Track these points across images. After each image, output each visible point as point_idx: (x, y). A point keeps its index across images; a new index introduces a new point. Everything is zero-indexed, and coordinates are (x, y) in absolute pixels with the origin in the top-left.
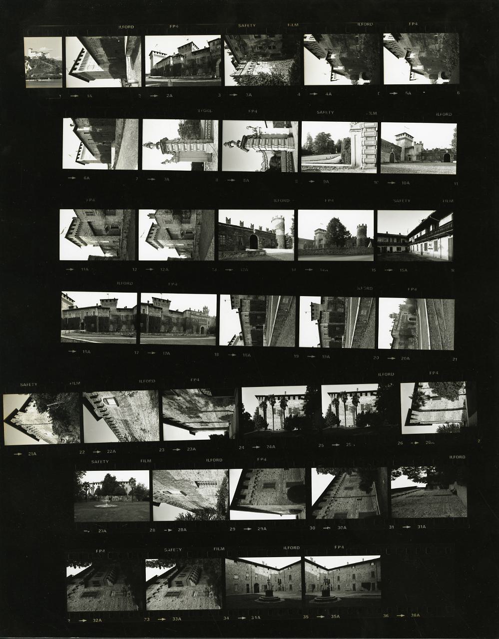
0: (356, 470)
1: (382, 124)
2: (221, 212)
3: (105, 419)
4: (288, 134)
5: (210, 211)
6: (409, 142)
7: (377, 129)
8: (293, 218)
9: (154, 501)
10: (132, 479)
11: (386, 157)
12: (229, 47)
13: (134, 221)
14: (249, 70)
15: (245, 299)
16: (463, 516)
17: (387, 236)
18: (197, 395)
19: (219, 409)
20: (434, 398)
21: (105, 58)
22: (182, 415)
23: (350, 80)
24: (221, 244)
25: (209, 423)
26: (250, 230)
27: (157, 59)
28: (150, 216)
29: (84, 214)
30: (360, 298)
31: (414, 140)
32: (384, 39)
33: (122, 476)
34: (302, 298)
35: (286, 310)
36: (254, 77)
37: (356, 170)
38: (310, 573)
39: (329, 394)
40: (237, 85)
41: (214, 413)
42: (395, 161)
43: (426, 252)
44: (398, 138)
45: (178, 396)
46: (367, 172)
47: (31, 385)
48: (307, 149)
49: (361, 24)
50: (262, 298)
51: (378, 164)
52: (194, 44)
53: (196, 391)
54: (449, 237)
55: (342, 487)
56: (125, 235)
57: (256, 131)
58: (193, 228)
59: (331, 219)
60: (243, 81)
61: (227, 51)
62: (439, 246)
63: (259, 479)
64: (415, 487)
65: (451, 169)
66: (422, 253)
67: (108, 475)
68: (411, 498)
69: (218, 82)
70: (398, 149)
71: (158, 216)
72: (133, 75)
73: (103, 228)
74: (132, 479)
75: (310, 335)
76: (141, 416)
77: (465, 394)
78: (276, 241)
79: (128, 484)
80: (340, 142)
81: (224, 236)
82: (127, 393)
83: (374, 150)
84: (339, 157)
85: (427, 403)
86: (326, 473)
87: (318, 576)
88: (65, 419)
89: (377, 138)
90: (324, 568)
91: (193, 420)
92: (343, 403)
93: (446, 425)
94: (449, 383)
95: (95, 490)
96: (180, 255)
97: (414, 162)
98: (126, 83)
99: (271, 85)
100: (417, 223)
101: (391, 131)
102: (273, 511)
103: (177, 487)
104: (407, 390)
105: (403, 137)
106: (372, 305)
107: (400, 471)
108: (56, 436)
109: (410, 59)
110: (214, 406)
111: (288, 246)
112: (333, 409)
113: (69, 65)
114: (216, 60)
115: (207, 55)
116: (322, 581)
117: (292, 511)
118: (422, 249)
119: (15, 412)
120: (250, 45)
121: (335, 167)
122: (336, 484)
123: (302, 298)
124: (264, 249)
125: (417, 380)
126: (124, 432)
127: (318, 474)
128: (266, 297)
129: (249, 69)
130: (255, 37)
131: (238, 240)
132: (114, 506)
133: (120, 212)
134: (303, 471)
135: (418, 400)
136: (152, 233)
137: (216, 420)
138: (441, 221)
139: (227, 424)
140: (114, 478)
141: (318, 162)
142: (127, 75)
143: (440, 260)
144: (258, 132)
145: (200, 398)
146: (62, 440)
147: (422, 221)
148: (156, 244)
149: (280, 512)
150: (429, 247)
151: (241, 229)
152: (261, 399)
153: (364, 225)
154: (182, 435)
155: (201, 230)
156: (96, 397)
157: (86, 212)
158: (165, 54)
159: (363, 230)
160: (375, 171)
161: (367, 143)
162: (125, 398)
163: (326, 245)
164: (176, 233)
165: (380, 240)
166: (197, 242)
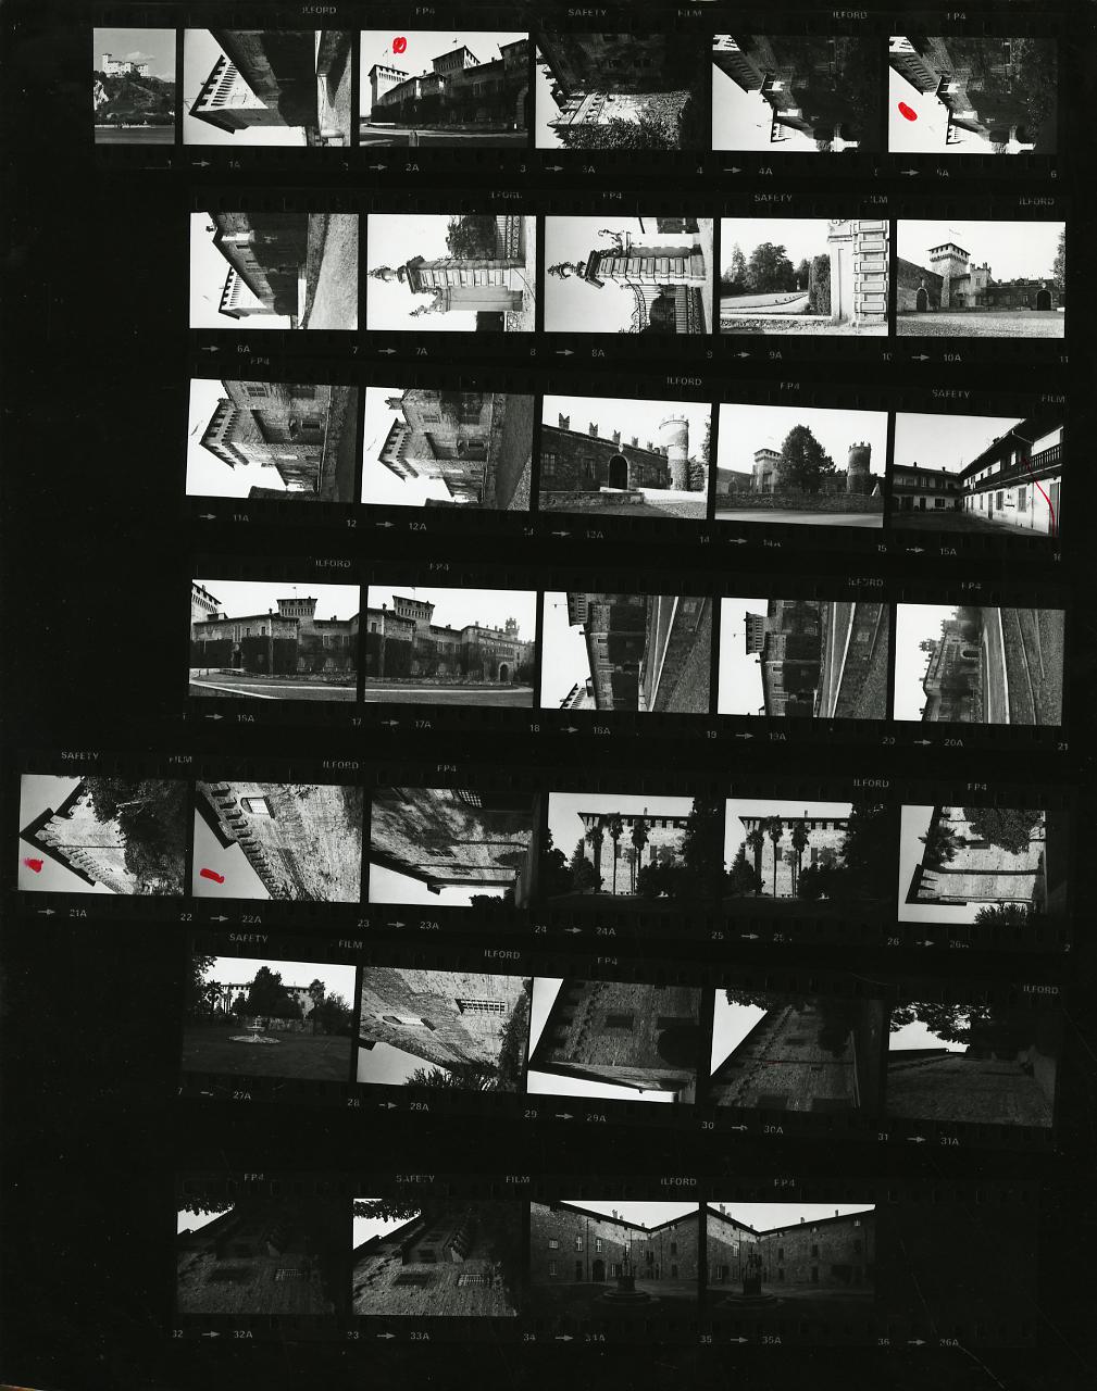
0: (815, 1001)
1: (900, 222)
2: (548, 400)
3: (243, 846)
4: (691, 247)
5: (524, 397)
6: (961, 264)
7: (888, 236)
8: (709, 421)
9: (361, 1036)
10: (317, 982)
11: (908, 299)
12: (546, 60)
13: (355, 414)
14: (589, 114)
15: (599, 603)
16: (1044, 1125)
17: (914, 471)
18: (449, 804)
19: (497, 838)
20: (975, 844)
21: (270, 80)
22: (412, 848)
23: (815, 141)
24: (546, 473)
25: (472, 868)
26: (611, 446)
27: (386, 85)
28: (392, 402)
29: (244, 391)
30: (854, 605)
31: (971, 260)
32: (892, 49)
33: (295, 974)
34: (725, 602)
35: (691, 630)
36: (602, 128)
37: (842, 327)
38: (717, 1241)
39: (742, 819)
40: (562, 146)
41: (485, 847)
42: (929, 307)
43: (1000, 511)
44: (935, 255)
45: (408, 803)
46: (867, 332)
47: (86, 756)
48: (732, 280)
49: (840, 15)
50: (635, 600)
51: (891, 316)
52: (468, 52)
53: (449, 794)
54: (1051, 481)
55: (781, 1038)
56: (333, 443)
57: (619, 240)
59: (791, 428)
60: (576, 138)
61: (541, 70)
62: (1028, 500)
63: (598, 1005)
64: (943, 1051)
65: (1051, 326)
66: (990, 514)
67: (265, 970)
68: (931, 1074)
69: (519, 139)
70: (935, 279)
71: (408, 404)
72: (331, 119)
73: (284, 425)
74: (317, 982)
75: (742, 688)
76: (323, 844)
77: (1042, 840)
78: (667, 472)
79: (308, 993)
80: (806, 265)
81: (553, 457)
82: (293, 789)
83: (881, 284)
84: (803, 300)
85: (957, 854)
86: (747, 1004)
87: (737, 1247)
88: (156, 840)
89: (888, 255)
90: (750, 1230)
91: (437, 859)
92: (772, 843)
93: (996, 906)
94: (1009, 811)
95: (233, 1000)
96: (452, 495)
97: (970, 310)
98: (317, 138)
99: (635, 147)
100: (984, 446)
101: (920, 240)
102: (623, 1080)
103: (414, 1009)
104: (915, 821)
105: (945, 252)
106: (882, 621)
107: (912, 1011)
108: (133, 877)
109: (947, 95)
110: (485, 831)
111: (693, 486)
112: (750, 854)
113: (191, 93)
114: (519, 88)
115: (498, 77)
116: (745, 1260)
117: (666, 1085)
118: (990, 506)
119: (47, 816)
120: (593, 57)
121: (796, 322)
122: (767, 1030)
123: (725, 602)
124: (641, 490)
125: (939, 801)
126: (281, 876)
127: (730, 1003)
128: (646, 601)
129: (591, 111)
130: (606, 39)
131: (583, 467)
132: (271, 1040)
133: (324, 390)
134: (697, 993)
135: (938, 844)
136: (394, 443)
137: (488, 862)
138: (1035, 443)
139: (513, 874)
140: (278, 977)
141: (759, 310)
142: (320, 118)
143: (1030, 533)
144: (624, 243)
145: (456, 811)
146: (144, 885)
147: (994, 441)
148: (401, 468)
149: (638, 1084)
150: (1006, 501)
151: (590, 443)
152: (591, 821)
153: (866, 445)
154: (411, 892)
155: (503, 441)
156: (225, 793)
157: (249, 389)
158: (404, 74)
159: (862, 456)
160: (883, 331)
161: (865, 266)
162: (289, 800)
163: (779, 486)
164: (447, 444)
165: (899, 481)
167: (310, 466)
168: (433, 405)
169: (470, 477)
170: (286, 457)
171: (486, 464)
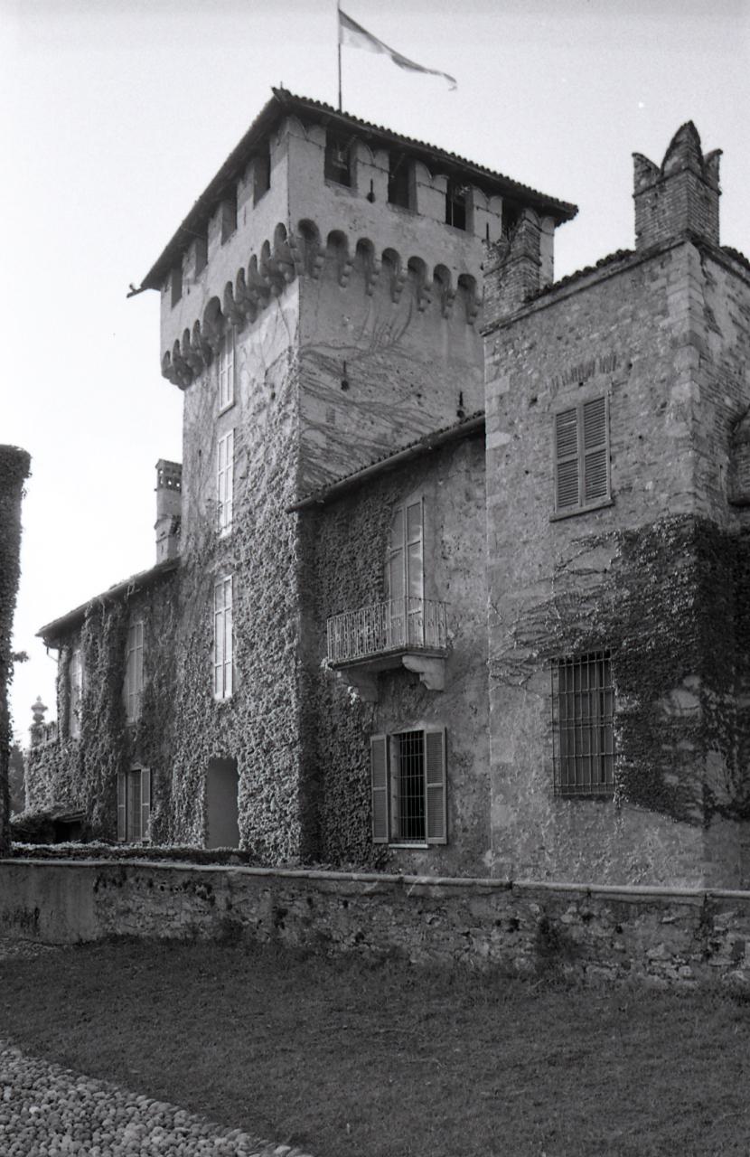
29: (581, 375)
58: (482, 840)
96: (60, 634)
136: (401, 196)
155: (448, 979)
164: (409, 580)
166: (257, 912)
167: (178, 788)
168: (681, 469)
169: (184, 764)
170: (224, 629)
171: (286, 864)
